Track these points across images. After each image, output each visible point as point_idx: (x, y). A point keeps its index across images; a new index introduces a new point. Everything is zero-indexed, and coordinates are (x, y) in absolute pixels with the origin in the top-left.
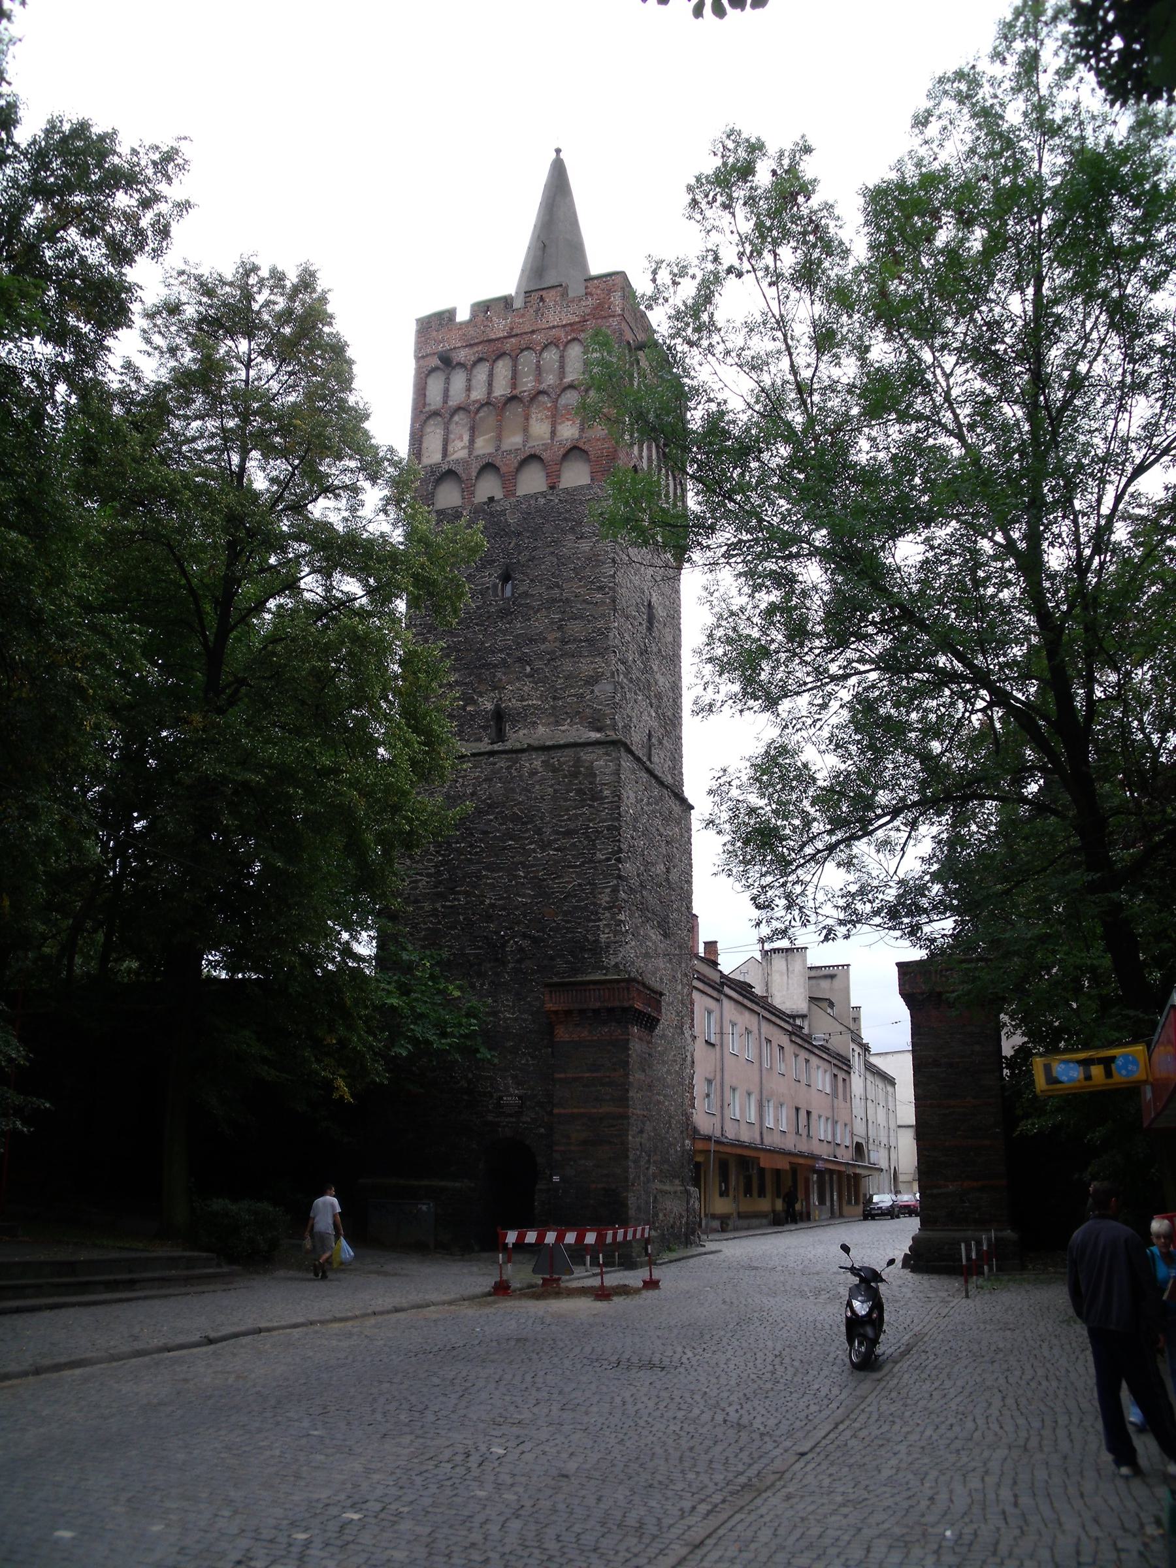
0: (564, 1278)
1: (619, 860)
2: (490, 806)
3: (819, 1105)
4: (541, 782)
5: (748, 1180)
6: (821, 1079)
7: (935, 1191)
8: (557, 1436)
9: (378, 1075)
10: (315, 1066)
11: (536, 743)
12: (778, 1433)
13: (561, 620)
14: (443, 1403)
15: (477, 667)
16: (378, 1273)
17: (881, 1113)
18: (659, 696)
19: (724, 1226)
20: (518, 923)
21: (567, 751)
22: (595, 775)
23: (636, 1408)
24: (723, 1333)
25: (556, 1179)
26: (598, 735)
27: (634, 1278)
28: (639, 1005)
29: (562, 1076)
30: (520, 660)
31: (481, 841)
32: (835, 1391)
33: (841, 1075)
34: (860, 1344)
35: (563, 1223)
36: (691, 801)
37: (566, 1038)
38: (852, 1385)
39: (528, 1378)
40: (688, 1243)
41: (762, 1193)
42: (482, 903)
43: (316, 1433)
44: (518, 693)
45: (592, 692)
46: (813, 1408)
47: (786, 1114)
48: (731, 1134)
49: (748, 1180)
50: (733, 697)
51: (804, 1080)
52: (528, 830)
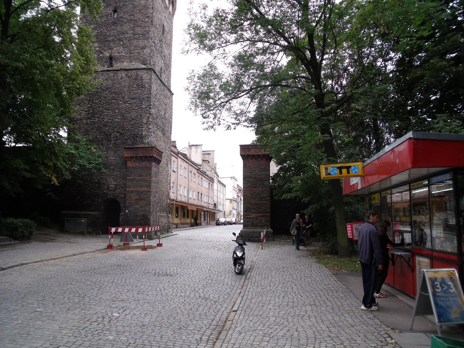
0: (130, 243)
1: (150, 108)
2: (107, 88)
3: (204, 192)
4: (124, 81)
5: (184, 213)
6: (205, 184)
7: (248, 217)
8: (138, 306)
9: (67, 176)
10: (44, 172)
11: (123, 68)
12: (220, 301)
13: (134, 27)
14: (92, 293)
15: (103, 41)
16: (68, 242)
17: (221, 195)
18: (165, 56)
19: (177, 226)
20: (115, 128)
21: (134, 71)
22: (143, 80)
23: (166, 292)
24: (188, 262)
25: (127, 211)
26: (145, 66)
27: (154, 243)
28: (155, 156)
29: (129, 178)
30: (119, 40)
31: (103, 100)
32: (233, 283)
33: (211, 183)
34: (239, 266)
35: (130, 226)
36: (173, 92)
37: (131, 165)
38: (239, 280)
39: (123, 280)
40: (168, 232)
41: (188, 217)
42: (103, 121)
43: (39, 310)
44: (117, 51)
45: (143, 52)
46: (229, 290)
47: (195, 194)
48: (179, 199)
49: (184, 213)
50: (195, 49)
51: (200, 184)
52: (119, 97)
